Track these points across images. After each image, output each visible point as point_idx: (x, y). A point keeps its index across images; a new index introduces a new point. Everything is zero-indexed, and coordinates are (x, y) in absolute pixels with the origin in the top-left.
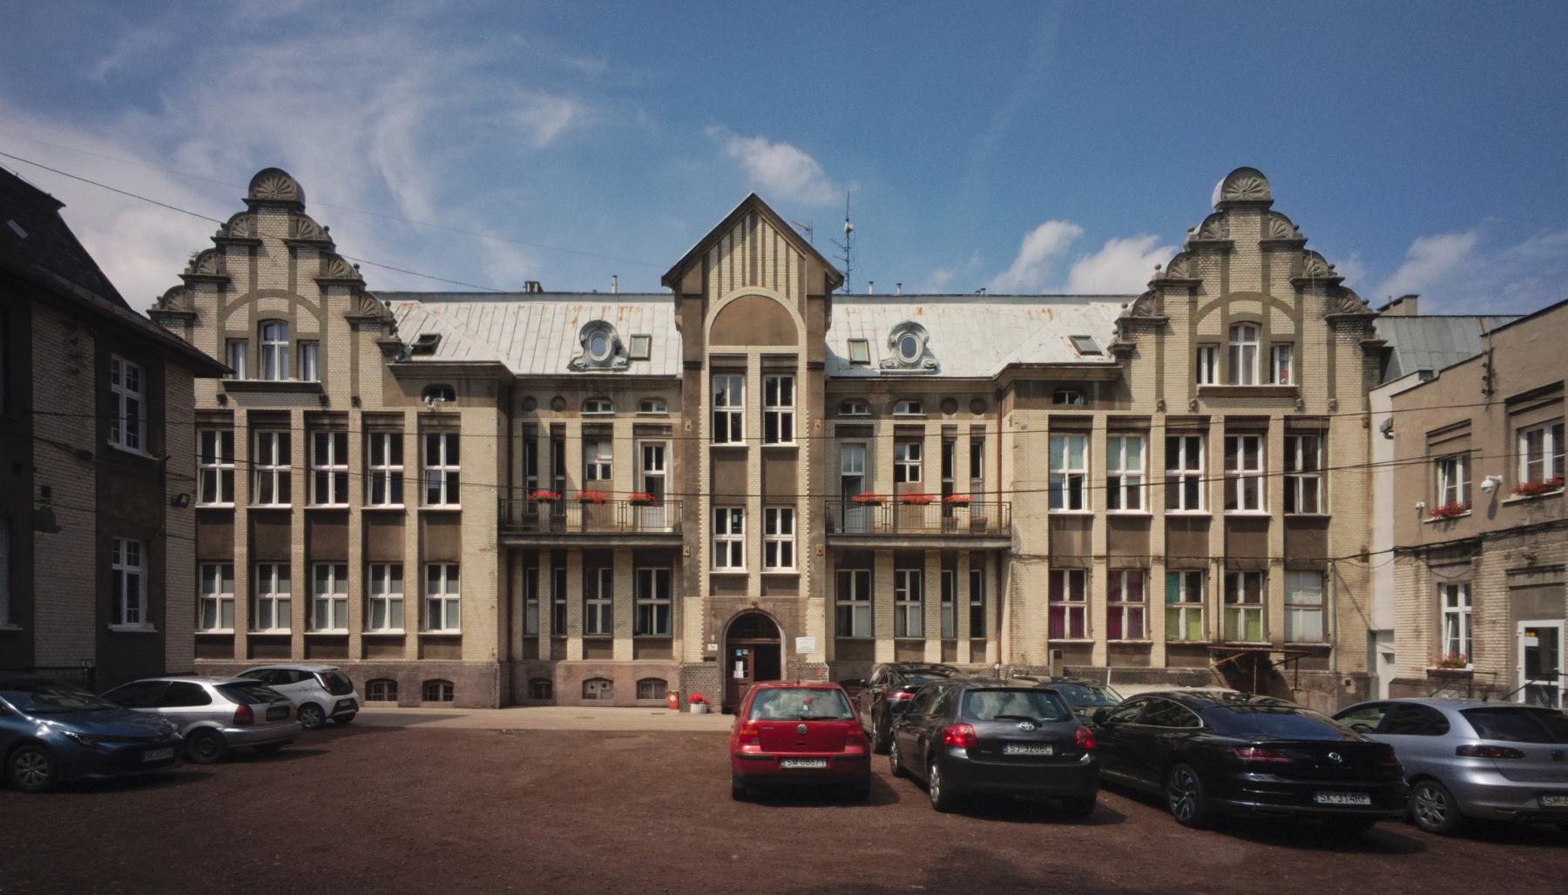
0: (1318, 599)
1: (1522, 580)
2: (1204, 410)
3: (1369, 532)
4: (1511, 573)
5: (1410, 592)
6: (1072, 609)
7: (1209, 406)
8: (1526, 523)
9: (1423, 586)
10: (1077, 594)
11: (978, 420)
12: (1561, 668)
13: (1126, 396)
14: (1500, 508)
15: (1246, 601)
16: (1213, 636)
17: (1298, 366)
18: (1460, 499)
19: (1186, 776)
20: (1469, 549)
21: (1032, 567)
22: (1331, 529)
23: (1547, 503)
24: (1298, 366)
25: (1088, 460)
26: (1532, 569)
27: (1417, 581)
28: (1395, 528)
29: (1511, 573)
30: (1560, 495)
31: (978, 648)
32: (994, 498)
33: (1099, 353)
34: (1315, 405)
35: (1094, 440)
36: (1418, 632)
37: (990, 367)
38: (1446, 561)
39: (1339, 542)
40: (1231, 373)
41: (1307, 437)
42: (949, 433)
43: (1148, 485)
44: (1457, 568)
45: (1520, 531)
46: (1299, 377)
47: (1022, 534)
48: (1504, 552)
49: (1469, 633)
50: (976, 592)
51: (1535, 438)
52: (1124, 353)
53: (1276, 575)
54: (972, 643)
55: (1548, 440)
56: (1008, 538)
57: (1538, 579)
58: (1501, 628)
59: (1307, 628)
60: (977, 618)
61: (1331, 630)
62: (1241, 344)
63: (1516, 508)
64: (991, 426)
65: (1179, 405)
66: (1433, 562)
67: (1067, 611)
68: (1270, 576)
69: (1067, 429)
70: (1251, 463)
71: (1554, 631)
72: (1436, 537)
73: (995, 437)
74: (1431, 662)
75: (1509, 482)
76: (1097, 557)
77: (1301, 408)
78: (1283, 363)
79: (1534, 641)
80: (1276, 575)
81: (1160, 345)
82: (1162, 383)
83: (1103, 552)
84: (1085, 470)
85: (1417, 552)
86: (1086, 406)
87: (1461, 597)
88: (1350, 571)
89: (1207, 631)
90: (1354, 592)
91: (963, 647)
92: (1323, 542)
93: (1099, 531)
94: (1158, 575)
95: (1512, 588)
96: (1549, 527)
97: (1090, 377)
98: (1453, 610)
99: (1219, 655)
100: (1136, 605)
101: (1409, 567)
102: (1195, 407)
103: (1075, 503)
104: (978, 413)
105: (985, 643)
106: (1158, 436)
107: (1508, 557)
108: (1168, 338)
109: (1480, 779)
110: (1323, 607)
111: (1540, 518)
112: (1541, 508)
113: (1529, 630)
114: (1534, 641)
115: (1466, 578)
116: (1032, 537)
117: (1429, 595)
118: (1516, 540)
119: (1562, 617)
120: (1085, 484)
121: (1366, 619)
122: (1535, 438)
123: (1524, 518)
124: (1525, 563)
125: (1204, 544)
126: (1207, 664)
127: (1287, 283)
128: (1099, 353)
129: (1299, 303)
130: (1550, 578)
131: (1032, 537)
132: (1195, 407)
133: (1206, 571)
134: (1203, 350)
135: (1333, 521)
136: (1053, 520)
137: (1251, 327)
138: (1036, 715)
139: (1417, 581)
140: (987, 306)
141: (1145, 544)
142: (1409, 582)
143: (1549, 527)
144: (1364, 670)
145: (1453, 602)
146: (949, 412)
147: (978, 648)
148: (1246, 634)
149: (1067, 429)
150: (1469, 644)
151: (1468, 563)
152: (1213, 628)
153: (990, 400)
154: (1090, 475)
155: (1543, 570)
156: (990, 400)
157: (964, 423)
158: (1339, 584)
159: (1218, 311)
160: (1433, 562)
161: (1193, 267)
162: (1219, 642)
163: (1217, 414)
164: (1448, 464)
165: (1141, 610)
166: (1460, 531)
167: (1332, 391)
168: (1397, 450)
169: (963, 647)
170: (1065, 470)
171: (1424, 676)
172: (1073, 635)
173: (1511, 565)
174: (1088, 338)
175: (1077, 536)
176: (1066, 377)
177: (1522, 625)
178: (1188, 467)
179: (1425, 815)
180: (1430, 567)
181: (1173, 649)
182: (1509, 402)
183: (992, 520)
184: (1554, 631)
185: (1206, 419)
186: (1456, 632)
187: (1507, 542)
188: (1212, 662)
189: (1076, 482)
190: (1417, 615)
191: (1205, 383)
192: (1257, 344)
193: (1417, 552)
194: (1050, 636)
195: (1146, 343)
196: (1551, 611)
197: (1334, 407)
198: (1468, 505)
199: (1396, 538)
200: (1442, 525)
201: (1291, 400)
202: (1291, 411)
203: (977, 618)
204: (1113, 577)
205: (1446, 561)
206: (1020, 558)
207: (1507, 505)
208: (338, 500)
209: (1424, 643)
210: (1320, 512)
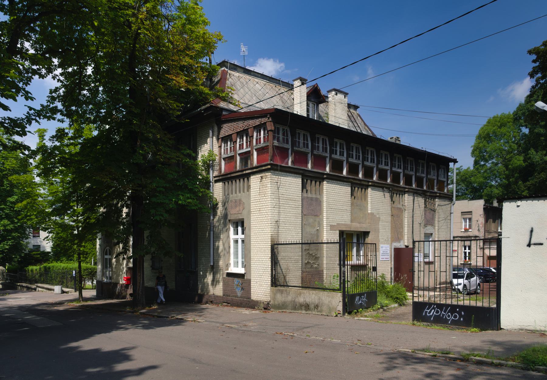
110: (419, 241)
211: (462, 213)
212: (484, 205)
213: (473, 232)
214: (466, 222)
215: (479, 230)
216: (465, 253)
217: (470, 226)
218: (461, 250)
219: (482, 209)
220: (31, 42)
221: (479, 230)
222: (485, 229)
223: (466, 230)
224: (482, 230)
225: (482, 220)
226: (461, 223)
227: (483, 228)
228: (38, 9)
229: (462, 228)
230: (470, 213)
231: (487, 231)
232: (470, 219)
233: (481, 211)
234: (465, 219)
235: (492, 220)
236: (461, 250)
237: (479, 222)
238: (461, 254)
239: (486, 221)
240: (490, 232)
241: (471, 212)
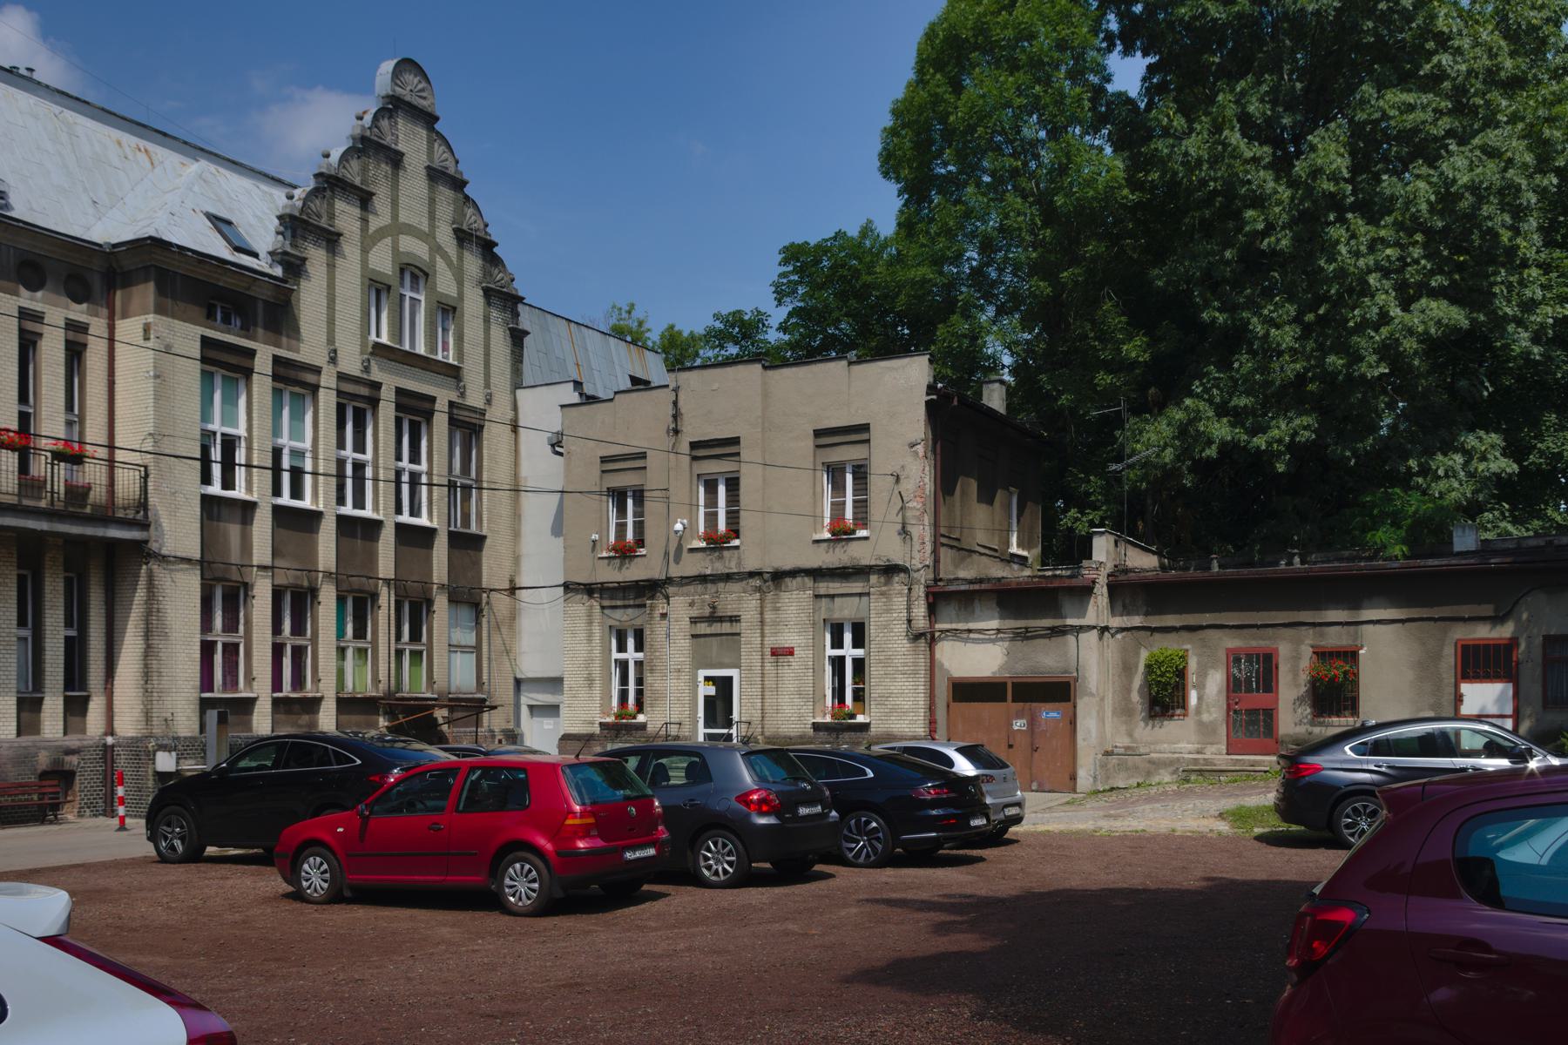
0: (470, 639)
1: (703, 628)
2: (376, 375)
3: (517, 560)
4: (694, 621)
5: (582, 636)
6: (225, 645)
7: (381, 370)
8: (708, 572)
9: (597, 629)
10: (231, 625)
11: (79, 312)
12: (735, 716)
13: (294, 333)
14: (685, 554)
15: (355, 637)
16: (383, 687)
17: (460, 339)
18: (630, 536)
19: (868, 823)
20: (648, 590)
21: (178, 576)
22: (486, 552)
23: (726, 553)
24: (460, 339)
25: (248, 415)
26: (713, 618)
27: (590, 623)
28: (565, 559)
29: (694, 621)
30: (737, 548)
31: (76, 708)
32: (102, 453)
33: (255, 255)
34: (475, 399)
35: (255, 389)
36: (590, 680)
37: (109, 229)
38: (619, 603)
39: (493, 570)
40: (397, 332)
41: (468, 428)
42: (30, 326)
43: (430, 485)
44: (630, 611)
45: (703, 579)
46: (460, 354)
47: (165, 523)
48: (689, 599)
49: (639, 681)
50: (76, 616)
51: (711, 487)
52: (294, 267)
53: (441, 603)
54: (67, 700)
55: (722, 489)
56: (145, 526)
57: (717, 628)
58: (685, 677)
59: (459, 675)
60: (75, 652)
61: (485, 677)
62: (409, 294)
63: (699, 555)
64: (98, 325)
65: (351, 363)
66: (606, 603)
67: (220, 647)
68: (435, 607)
69: (226, 366)
70: (360, 446)
71: (730, 679)
72: (611, 574)
73: (104, 344)
74: (605, 713)
75: (690, 528)
76: (262, 568)
77: (463, 395)
78: (445, 330)
79: (711, 690)
80: (441, 603)
81: (331, 267)
82: (333, 321)
83: (267, 560)
84: (241, 431)
85: (589, 590)
86: (246, 330)
87: (631, 643)
88: (500, 603)
89: (376, 681)
90: (504, 630)
91: (53, 705)
92: (477, 564)
93: (262, 525)
94: (328, 596)
95: (693, 636)
96: (728, 577)
97: (255, 292)
98: (622, 656)
99: (391, 712)
100: (299, 641)
101: (581, 607)
102: (367, 369)
103: (228, 483)
104: (78, 300)
105: (86, 700)
106: (327, 400)
107: (691, 604)
108: (339, 261)
109: (763, 821)
110: (477, 648)
111: (720, 568)
112: (721, 558)
113: (707, 679)
114: (711, 690)
115: (638, 622)
116: (178, 530)
117: (602, 639)
118: (700, 588)
119: (737, 666)
120: (369, 472)
121: (513, 663)
122: (711, 487)
123: (706, 565)
124: (707, 611)
125: (372, 558)
126: (375, 725)
127: (450, 230)
128: (255, 255)
129: (460, 258)
130: (726, 628)
131: (178, 530)
132: (367, 369)
133: (375, 596)
134: (377, 288)
135: (488, 542)
136: (207, 500)
137: (416, 273)
138: (766, 785)
139: (590, 623)
140: (56, 109)
141: (311, 552)
142: (581, 625)
143: (728, 577)
144: (511, 727)
145: (622, 648)
146: (33, 288)
147: (76, 708)
148: (415, 685)
149: (226, 366)
150: (640, 694)
151: (644, 606)
152: (383, 675)
153: (97, 284)
154: (249, 440)
155: (721, 619)
156: (97, 284)
157: (57, 312)
158: (493, 623)
159: (388, 240)
160: (606, 603)
161: (364, 170)
162: (389, 695)
163: (390, 380)
164: (619, 496)
165: (236, 646)
166: (635, 572)
167: (331, 340)
168: (568, 469)
169: (53, 705)
170: (216, 426)
171: (597, 730)
172: (294, 689)
173: (695, 613)
174: (229, 223)
175: (234, 530)
176: (224, 281)
177: (702, 673)
178: (355, 450)
179: (709, 868)
180: (603, 608)
181: (346, 704)
182: (694, 445)
183: (98, 494)
184: (730, 679)
185: (377, 386)
186: (624, 680)
187: (691, 588)
188: (383, 722)
189: (229, 444)
190: (589, 662)
191: (373, 337)
192: (422, 298)
193: (589, 590)
194: (202, 691)
195: (316, 257)
196: (727, 660)
197: (489, 402)
198: (640, 542)
199: (566, 571)
200: (618, 561)
201: (452, 381)
202: (455, 399)
203: (75, 652)
204: (277, 594)
205: (619, 603)
206: (163, 559)
207: (692, 550)
208: (355, 506)
209: (597, 692)
210: (474, 529)
211: (818, 433)
212: (931, 389)
213: (878, 543)
214: (838, 487)
215: (904, 532)
216: (838, 663)
217: (861, 506)
218: (818, 648)
219: (921, 412)
220: (1279, 153)
221: (904, 532)
222: (936, 525)
223: (841, 534)
224: (922, 532)
225: (919, 474)
226: (817, 498)
227: (927, 520)
228: (1319, 318)
229: (817, 518)
230: (859, 432)
231: (947, 540)
232: (861, 474)
233: (916, 425)
234: (835, 473)
235: (973, 485)
236: (818, 648)
237: (908, 486)
238: (817, 672)
239: (946, 483)
240: (965, 552)
241: (865, 428)
